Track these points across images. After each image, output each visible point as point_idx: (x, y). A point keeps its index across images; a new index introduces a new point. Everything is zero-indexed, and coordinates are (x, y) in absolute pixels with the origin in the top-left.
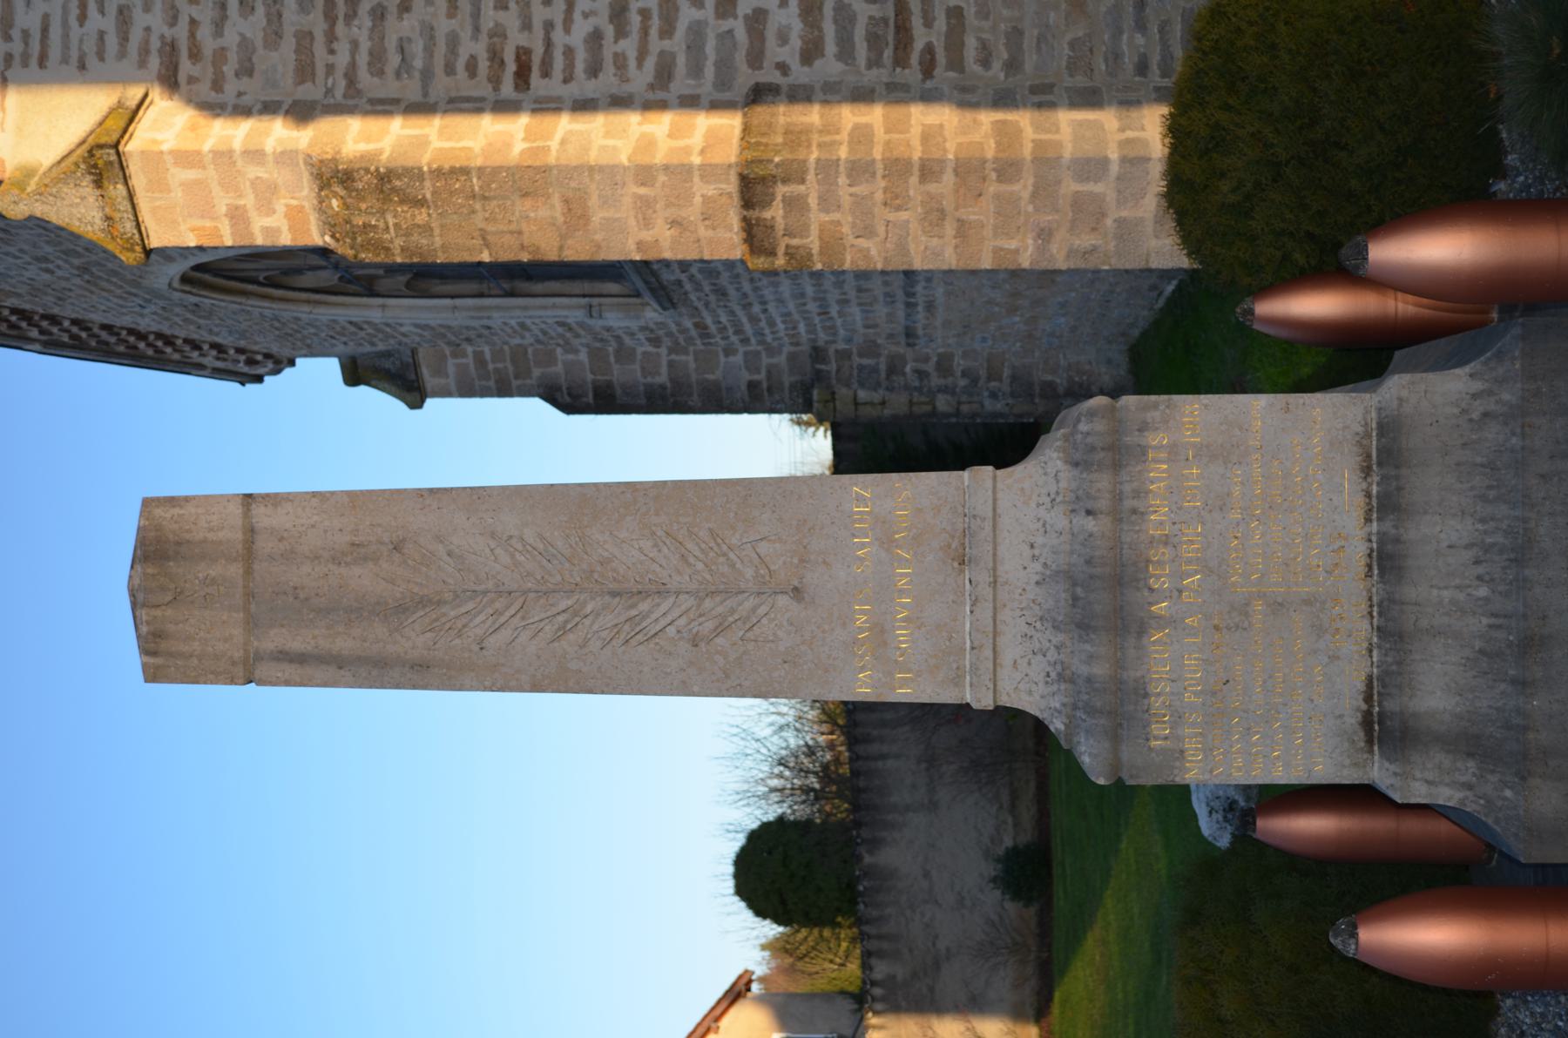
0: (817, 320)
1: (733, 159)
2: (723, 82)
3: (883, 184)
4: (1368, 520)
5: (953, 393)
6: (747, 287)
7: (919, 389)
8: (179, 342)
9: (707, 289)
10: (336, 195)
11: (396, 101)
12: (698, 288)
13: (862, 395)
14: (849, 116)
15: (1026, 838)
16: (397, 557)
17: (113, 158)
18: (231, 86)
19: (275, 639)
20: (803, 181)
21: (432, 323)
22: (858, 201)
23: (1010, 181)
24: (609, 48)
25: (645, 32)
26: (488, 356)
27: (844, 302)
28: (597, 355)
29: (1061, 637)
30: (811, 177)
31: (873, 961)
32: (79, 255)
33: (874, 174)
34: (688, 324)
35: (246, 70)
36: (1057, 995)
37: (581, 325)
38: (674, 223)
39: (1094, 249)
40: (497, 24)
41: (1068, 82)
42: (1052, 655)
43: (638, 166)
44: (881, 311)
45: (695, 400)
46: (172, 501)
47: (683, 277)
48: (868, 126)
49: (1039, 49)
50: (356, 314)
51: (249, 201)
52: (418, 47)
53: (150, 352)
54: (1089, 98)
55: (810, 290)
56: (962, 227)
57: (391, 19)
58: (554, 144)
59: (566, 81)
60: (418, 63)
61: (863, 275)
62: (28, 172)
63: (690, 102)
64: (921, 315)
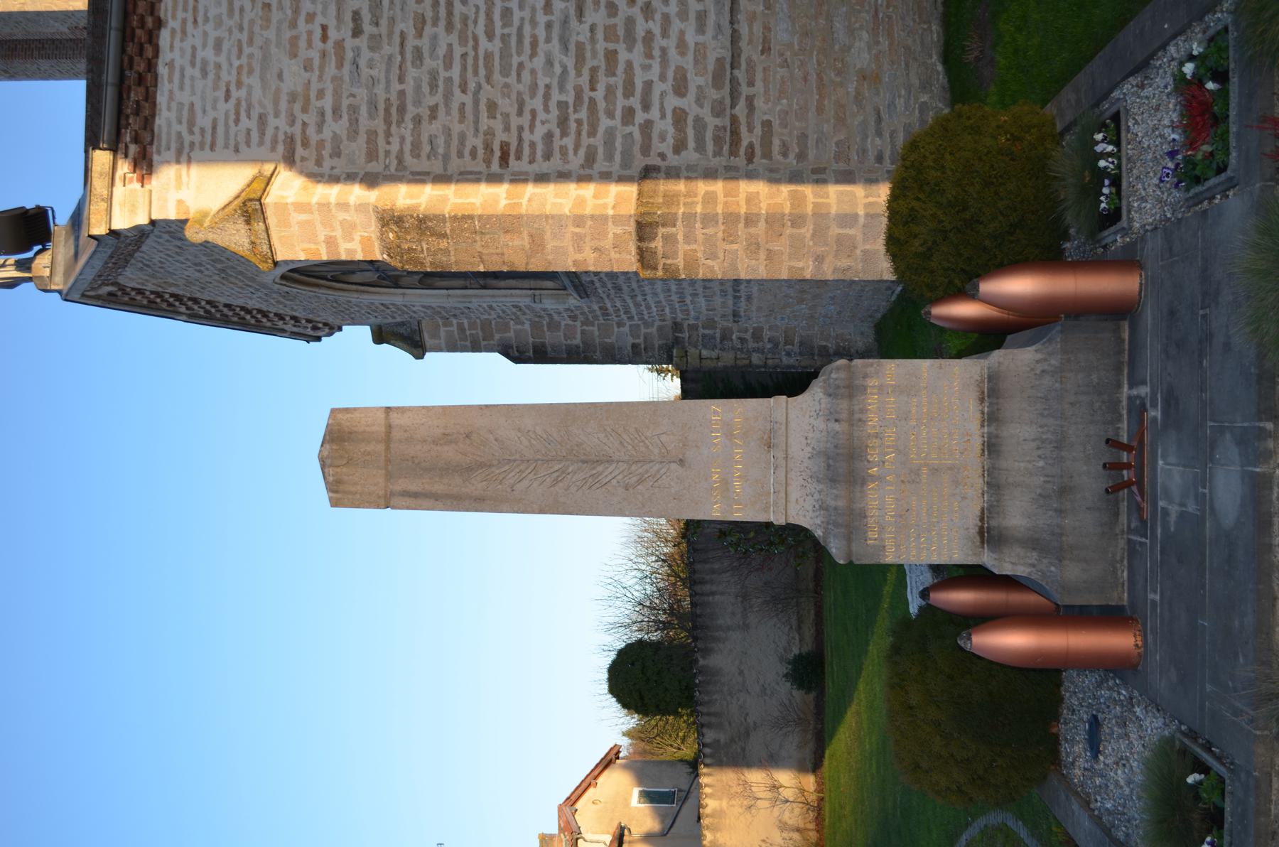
0: (677, 306)
1: (633, 212)
2: (626, 164)
3: (722, 228)
4: (982, 426)
5: (763, 353)
6: (634, 285)
7: (741, 350)
8: (271, 315)
9: (610, 286)
10: (392, 231)
11: (428, 173)
12: (604, 285)
13: (705, 353)
14: (702, 187)
15: (808, 647)
16: (468, 441)
17: (258, 207)
18: (327, 163)
19: (401, 485)
20: (674, 226)
21: (434, 305)
22: (708, 238)
23: (799, 227)
24: (557, 143)
25: (579, 133)
26: (466, 326)
27: (695, 295)
28: (536, 326)
29: (821, 486)
30: (679, 223)
31: (705, 730)
32: (222, 262)
33: (717, 222)
34: (596, 307)
35: (336, 153)
36: (827, 753)
37: (528, 307)
38: (596, 249)
39: (850, 268)
40: (489, 128)
41: (835, 166)
42: (817, 496)
43: (576, 217)
44: (718, 300)
45: (598, 355)
46: (347, 410)
47: (595, 279)
48: (714, 193)
49: (817, 146)
50: (386, 299)
51: (338, 233)
52: (441, 141)
53: (253, 321)
54: (846, 177)
55: (674, 288)
56: (770, 255)
57: (425, 123)
58: (524, 201)
59: (530, 162)
60: (441, 151)
61: (707, 282)
62: (205, 215)
63: (606, 177)
64: (743, 304)
